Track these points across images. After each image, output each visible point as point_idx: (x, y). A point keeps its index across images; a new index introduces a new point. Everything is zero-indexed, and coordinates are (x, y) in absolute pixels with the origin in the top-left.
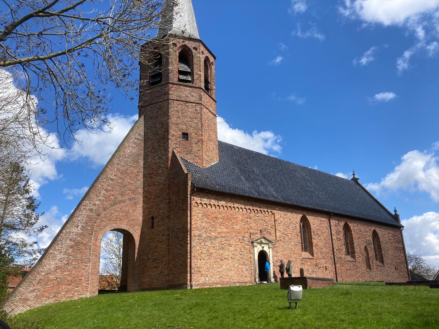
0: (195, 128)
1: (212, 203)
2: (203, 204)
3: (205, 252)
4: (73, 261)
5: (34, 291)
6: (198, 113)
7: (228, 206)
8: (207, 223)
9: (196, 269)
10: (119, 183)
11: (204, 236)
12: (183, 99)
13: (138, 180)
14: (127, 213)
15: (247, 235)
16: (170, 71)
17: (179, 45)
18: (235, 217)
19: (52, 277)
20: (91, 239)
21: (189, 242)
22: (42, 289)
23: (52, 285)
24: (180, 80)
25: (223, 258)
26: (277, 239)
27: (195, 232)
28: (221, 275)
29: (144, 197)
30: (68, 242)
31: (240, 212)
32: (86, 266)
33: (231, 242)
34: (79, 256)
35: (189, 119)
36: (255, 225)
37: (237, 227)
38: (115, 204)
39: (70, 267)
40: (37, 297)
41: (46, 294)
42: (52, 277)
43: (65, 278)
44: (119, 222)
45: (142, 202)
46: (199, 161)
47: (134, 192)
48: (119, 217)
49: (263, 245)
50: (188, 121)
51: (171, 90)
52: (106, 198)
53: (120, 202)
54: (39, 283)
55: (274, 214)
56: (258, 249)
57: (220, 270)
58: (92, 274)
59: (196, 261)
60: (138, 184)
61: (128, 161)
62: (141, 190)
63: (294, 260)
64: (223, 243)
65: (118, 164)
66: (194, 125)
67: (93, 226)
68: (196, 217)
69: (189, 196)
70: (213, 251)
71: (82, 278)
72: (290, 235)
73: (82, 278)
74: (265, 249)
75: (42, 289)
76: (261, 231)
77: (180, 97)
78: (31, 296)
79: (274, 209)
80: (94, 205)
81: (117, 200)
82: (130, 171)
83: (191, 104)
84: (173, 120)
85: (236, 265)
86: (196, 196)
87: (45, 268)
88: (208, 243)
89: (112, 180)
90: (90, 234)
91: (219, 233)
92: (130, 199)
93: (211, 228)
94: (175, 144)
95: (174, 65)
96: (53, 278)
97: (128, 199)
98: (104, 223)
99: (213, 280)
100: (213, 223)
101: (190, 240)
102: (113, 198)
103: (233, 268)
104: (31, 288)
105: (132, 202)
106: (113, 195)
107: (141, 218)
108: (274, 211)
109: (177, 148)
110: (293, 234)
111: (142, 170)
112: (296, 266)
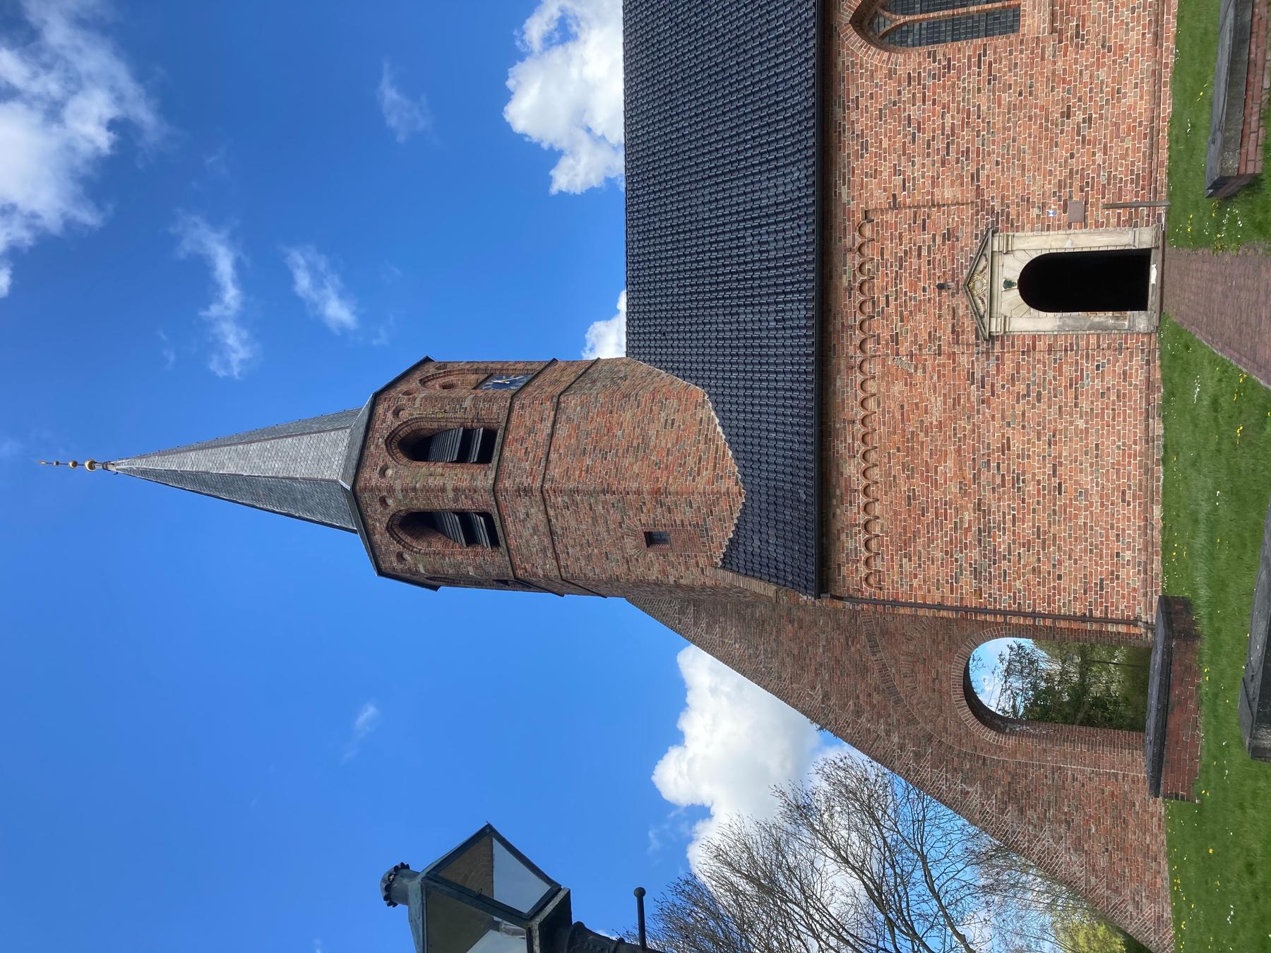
1: (862, 518)
2: (865, 482)
3: (1033, 559)
5: (1137, 905)
7: (863, 448)
8: (931, 541)
9: (1091, 596)
11: (975, 553)
12: (547, 541)
15: (964, 360)
17: (396, 547)
19: (1102, 862)
23: (1124, 863)
24: (481, 445)
28: (1116, 497)
30: (1008, 818)
32: (1074, 779)
33: (995, 441)
35: (601, 529)
36: (920, 317)
37: (937, 408)
38: (892, 691)
39: (1078, 819)
40: (1153, 897)
42: (1102, 862)
43: (1108, 832)
44: (945, 685)
46: (723, 504)
50: (608, 531)
52: (879, 716)
57: (1096, 499)
58: (1097, 765)
59: (1064, 598)
60: (826, 624)
61: (766, 650)
63: (1060, 92)
64: (998, 480)
66: (615, 516)
67: (963, 756)
68: (915, 583)
71: (1108, 789)
73: (1108, 789)
74: (1015, 276)
75: (1134, 885)
77: (544, 550)
78: (1149, 911)
81: (882, 686)
82: (792, 644)
83: (554, 520)
85: (1081, 424)
87: (1078, 874)
88: (1002, 541)
89: (826, 696)
92: (874, 648)
94: (687, 568)
95: (447, 483)
97: (874, 654)
98: (952, 726)
99: (1132, 532)
100: (931, 515)
101: (995, 612)
102: (876, 698)
106: (869, 695)
110: (946, 99)
112: (1086, 78)
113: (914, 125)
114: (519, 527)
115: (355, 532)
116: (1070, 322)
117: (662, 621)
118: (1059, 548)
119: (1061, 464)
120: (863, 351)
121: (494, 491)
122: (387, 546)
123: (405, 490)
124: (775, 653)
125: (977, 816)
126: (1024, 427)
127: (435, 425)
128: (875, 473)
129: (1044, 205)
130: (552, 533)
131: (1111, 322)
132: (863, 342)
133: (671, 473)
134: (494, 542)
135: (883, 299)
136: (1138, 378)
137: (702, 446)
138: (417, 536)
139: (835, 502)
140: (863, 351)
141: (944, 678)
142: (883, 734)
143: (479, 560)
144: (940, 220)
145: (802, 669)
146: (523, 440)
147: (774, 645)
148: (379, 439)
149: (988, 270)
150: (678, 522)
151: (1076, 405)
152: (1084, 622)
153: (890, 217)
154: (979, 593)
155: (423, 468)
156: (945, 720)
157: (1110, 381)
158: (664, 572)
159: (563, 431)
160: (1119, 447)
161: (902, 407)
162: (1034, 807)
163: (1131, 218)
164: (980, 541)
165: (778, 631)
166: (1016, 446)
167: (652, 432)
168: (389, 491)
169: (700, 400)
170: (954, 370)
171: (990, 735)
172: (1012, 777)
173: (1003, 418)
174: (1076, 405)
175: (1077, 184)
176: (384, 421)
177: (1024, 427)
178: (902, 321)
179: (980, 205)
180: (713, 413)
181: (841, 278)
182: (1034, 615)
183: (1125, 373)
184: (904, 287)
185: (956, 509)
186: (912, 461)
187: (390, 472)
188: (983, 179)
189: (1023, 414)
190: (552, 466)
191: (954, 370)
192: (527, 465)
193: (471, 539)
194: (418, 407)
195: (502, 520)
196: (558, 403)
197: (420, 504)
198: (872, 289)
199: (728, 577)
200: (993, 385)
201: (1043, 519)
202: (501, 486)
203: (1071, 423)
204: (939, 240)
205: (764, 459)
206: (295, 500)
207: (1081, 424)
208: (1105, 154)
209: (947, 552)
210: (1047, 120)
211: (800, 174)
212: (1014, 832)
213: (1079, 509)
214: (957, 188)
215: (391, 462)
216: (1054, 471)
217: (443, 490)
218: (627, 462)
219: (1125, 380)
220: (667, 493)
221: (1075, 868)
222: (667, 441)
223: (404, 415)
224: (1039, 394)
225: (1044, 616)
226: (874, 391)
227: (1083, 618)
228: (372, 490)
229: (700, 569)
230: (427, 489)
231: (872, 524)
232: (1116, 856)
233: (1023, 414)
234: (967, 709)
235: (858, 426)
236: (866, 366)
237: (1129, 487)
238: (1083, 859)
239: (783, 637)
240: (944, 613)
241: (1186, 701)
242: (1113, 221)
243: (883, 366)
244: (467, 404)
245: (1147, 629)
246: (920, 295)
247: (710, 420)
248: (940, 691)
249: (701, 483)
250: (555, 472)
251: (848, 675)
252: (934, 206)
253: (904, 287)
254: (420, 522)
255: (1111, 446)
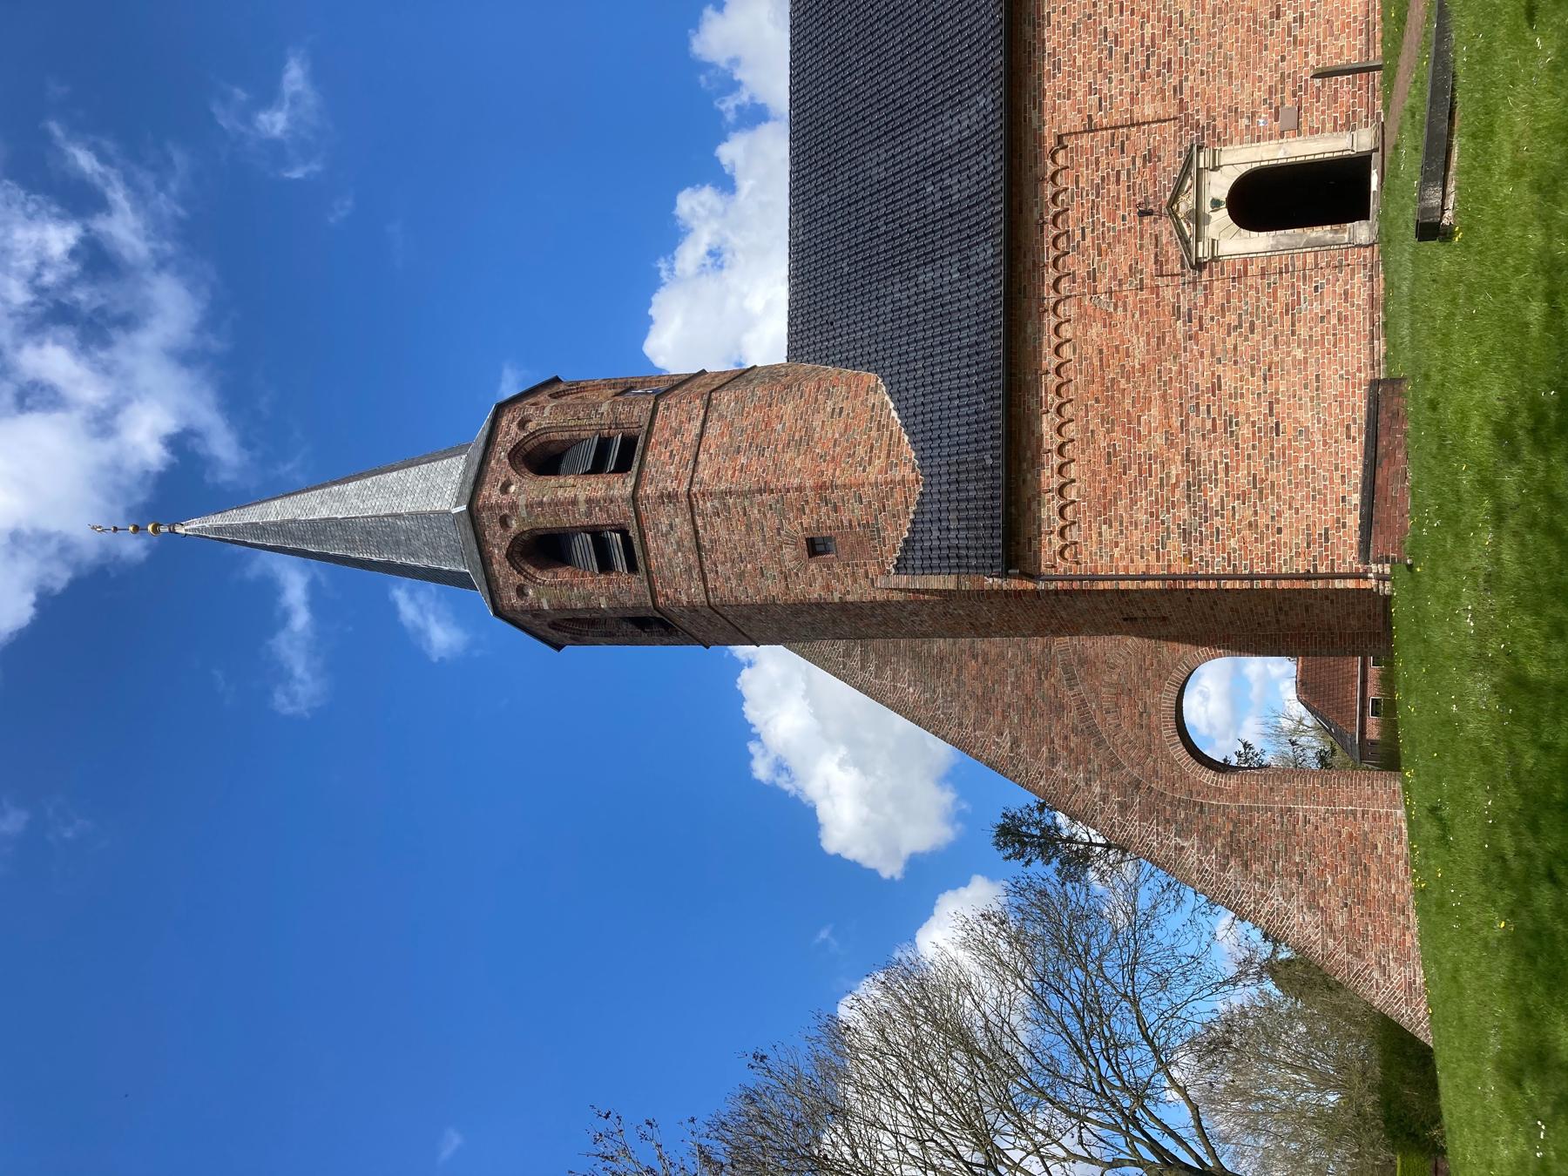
0: (783, 515)
1: (1055, 482)
2: (1059, 440)
4: (1289, 860)
6: (727, 508)
7: (1057, 401)
8: (1133, 502)
9: (1316, 550)
10: (1021, 720)
11: (1184, 512)
12: (693, 558)
13: (1002, 656)
14: (1120, 691)
15: (1168, 294)
16: (614, 604)
17: (517, 579)
18: (1096, 363)
19: (1341, 920)
20: (1218, 807)
21: (1213, 585)
22: (1379, 946)
23: (1366, 919)
24: (620, 453)
25: (1272, 421)
26: (1173, 111)
27: (1175, 558)
28: (1340, 434)
29: (1057, 633)
30: (1230, 875)
31: (1079, 334)
32: (1306, 821)
34: (1275, 844)
36: (1119, 248)
37: (1139, 349)
38: (1092, 731)
39: (1311, 868)
40: (1402, 960)
41: (1396, 934)
42: (1341, 920)
43: (1346, 882)
44: (1154, 718)
45: (1075, 640)
46: (898, 495)
47: (1044, 671)
48: (1136, 718)
49: (1207, 208)
50: (764, 540)
51: (679, 601)
52: (1078, 763)
53: (1085, 716)
54: (1359, 954)
55: (1060, 138)
56: (1230, 240)
57: (1318, 437)
59: (1286, 554)
60: (1015, 656)
61: (945, 693)
62: (1036, 645)
64: (1209, 425)
65: (961, 724)
66: (772, 521)
67: (1176, 804)
68: (1117, 552)
69: (1041, 586)
70: (1243, 472)
71: (1345, 832)
72: (1148, 30)
73: (1345, 832)
75: (1379, 946)
76: (1143, 214)
77: (689, 570)
78: (1398, 975)
79: (1040, 139)
80: (1105, 798)
82: (976, 684)
84: (773, 588)
85: (1299, 354)
86: (1037, 554)
87: (1313, 938)
88: (1214, 495)
89: (1015, 743)
90: (1201, 811)
91: (1171, 444)
92: (1071, 680)
93: (1154, 482)
94: (855, 581)
95: (579, 495)
96: (1346, 915)
98: (1163, 768)
100: (1133, 472)
101: (1207, 578)
102: (1074, 741)
103: (1312, 370)
104: (1376, 975)
105: (1080, 673)
107: (1132, 641)
108: (1050, 142)
109: (866, 573)
111: (964, 642)
113: (1111, 38)
114: (661, 542)
115: (461, 580)
116: (1284, 240)
117: (823, 668)
118: (1279, 498)
119: (1278, 401)
120: (1057, 291)
121: (634, 498)
122: (506, 578)
123: (529, 506)
124: (956, 695)
125: (1194, 876)
126: (1236, 363)
127: (566, 435)
128: (1071, 430)
129: (1253, 114)
130: (699, 547)
131: (1329, 236)
132: (1057, 281)
133: (838, 464)
134: (632, 567)
135: (1078, 232)
136: (1361, 297)
137: (874, 434)
138: (541, 567)
139: (1025, 466)
140: (1057, 291)
141: (1153, 710)
142: (1082, 784)
143: (613, 588)
144: (1140, 140)
145: (987, 712)
146: (667, 443)
147: (954, 685)
148: (501, 453)
149: (1193, 191)
150: (846, 523)
151: (1293, 333)
152: (1308, 579)
153: (1085, 141)
154: (1188, 557)
155: (553, 481)
156: (1155, 761)
157: (1330, 302)
158: (828, 587)
159: (714, 429)
160: (1341, 377)
161: (1101, 352)
162: (1260, 860)
163: (1348, 121)
164: (1189, 497)
165: (960, 669)
166: (1228, 384)
167: (817, 423)
168: (511, 508)
169: (872, 385)
170: (1158, 305)
171: (1208, 776)
172: (1235, 826)
173: (1213, 354)
174: (1293, 333)
175: (1289, 88)
176: (507, 433)
177: (1236, 363)
178: (1100, 255)
179: (1183, 118)
180: (887, 398)
181: (1031, 211)
182: (1252, 577)
183: (1346, 293)
184: (1102, 217)
185: (1163, 463)
186: (1113, 412)
187: (512, 489)
188: (1187, 91)
189: (1235, 348)
190: (700, 468)
191: (1158, 305)
192: (672, 469)
193: (606, 565)
194: (545, 417)
195: (643, 536)
196: (709, 399)
197: (546, 522)
198: (1066, 221)
199: (903, 581)
200: (1201, 318)
201: (1259, 466)
202: (641, 493)
203: (1289, 354)
204: (1139, 162)
205: (945, 433)
206: (397, 543)
207: (1299, 354)
208: (1318, 54)
209: (1152, 514)
210: (1255, 22)
211: (987, 101)
212: (1238, 892)
213: (1297, 450)
214: (1158, 104)
215: (514, 477)
216: (1271, 410)
217: (574, 502)
218: (787, 457)
219: (1346, 300)
220: (834, 486)
221: (1310, 930)
222: (835, 430)
223: (531, 426)
224: (1252, 324)
225: (1263, 578)
226: (1069, 335)
227: (1307, 576)
228: (491, 508)
229: (875, 580)
230: (555, 503)
231: (1068, 488)
232: (1358, 910)
233: (1235, 348)
234: (1181, 746)
235: (1052, 376)
236: (1061, 308)
237: (1354, 421)
238: (1319, 918)
239: (965, 677)
240: (1150, 584)
241: (1394, 450)
242: (1329, 126)
243: (1080, 307)
244: (605, 408)
245: (1378, 580)
246: (1119, 225)
247: (884, 405)
248: (1148, 726)
249: (873, 473)
250: (705, 473)
251: (1041, 716)
252: (1133, 125)
253: (1102, 217)
254: (546, 548)
255: (1332, 375)
